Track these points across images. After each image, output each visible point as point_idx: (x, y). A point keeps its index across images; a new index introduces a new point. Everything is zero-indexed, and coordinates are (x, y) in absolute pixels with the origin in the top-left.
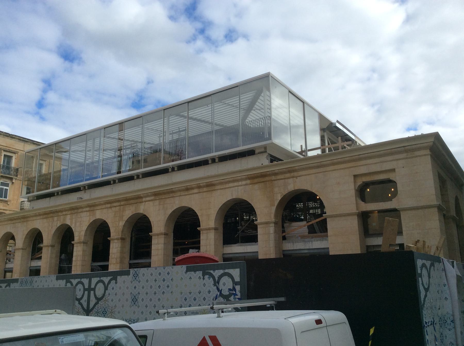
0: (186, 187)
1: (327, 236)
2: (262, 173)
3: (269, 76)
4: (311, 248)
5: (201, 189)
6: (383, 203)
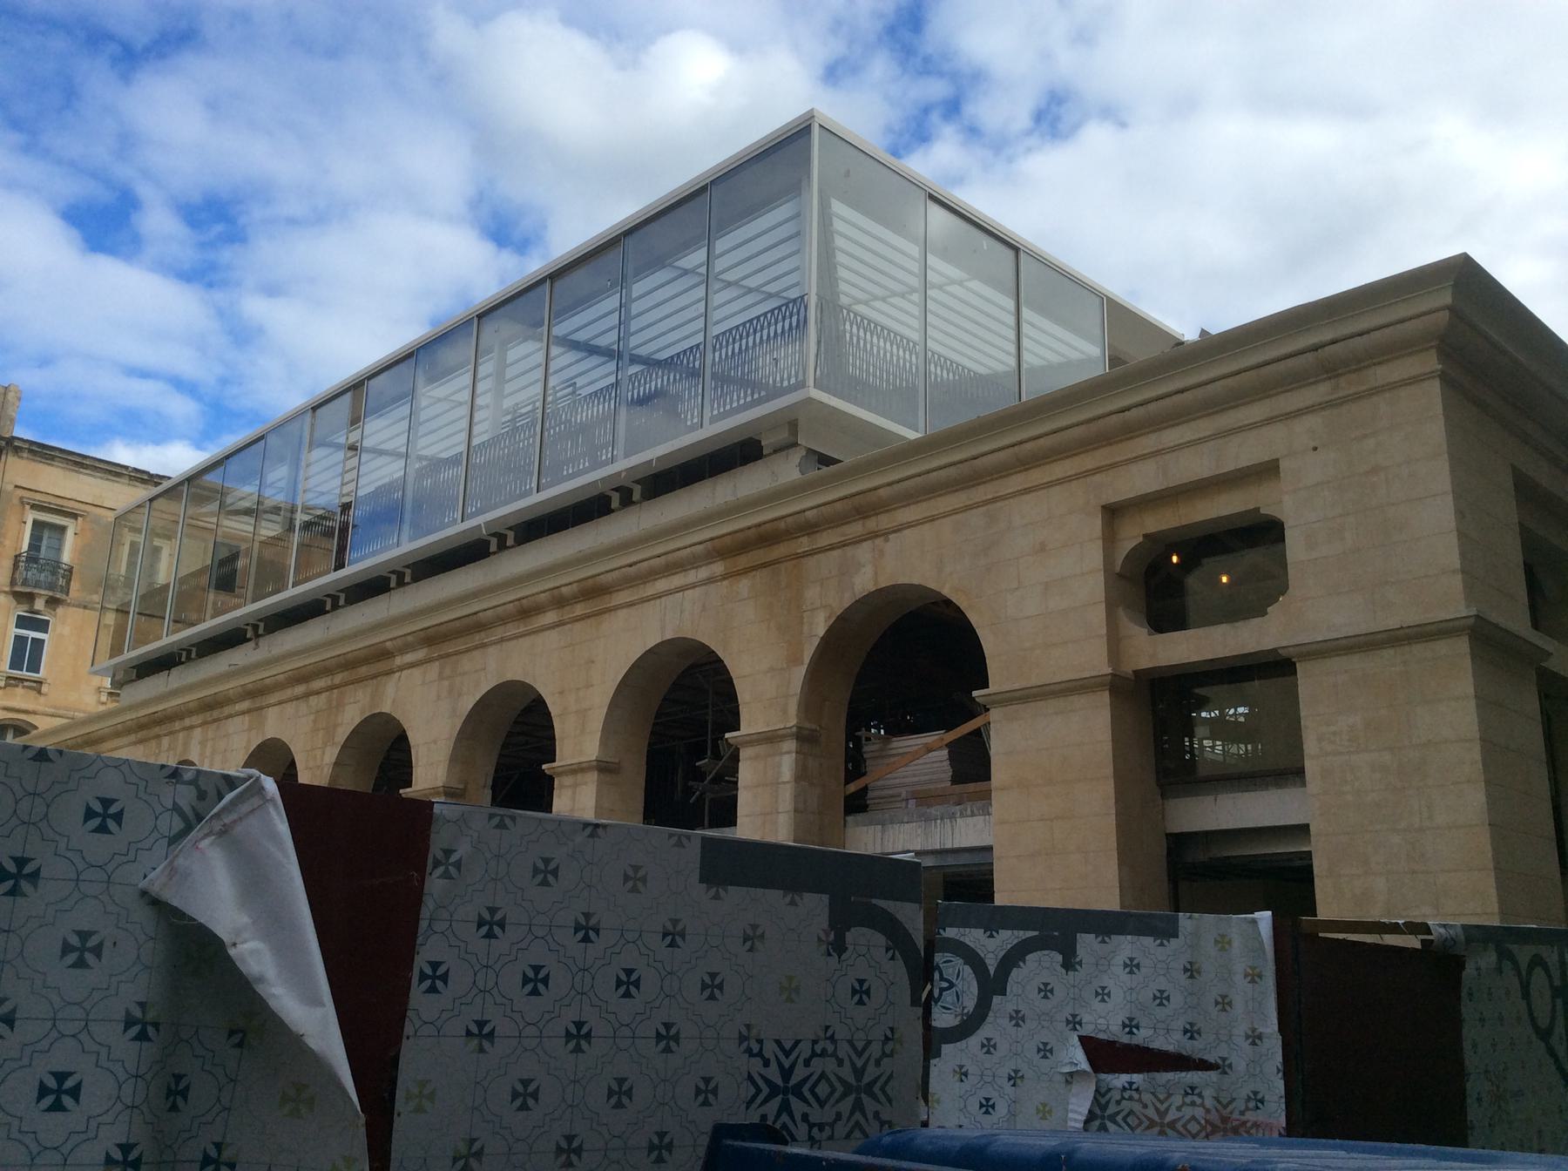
0: (516, 603)
1: (986, 796)
3: (810, 125)
4: (949, 846)
5: (568, 608)
6: (1224, 626)
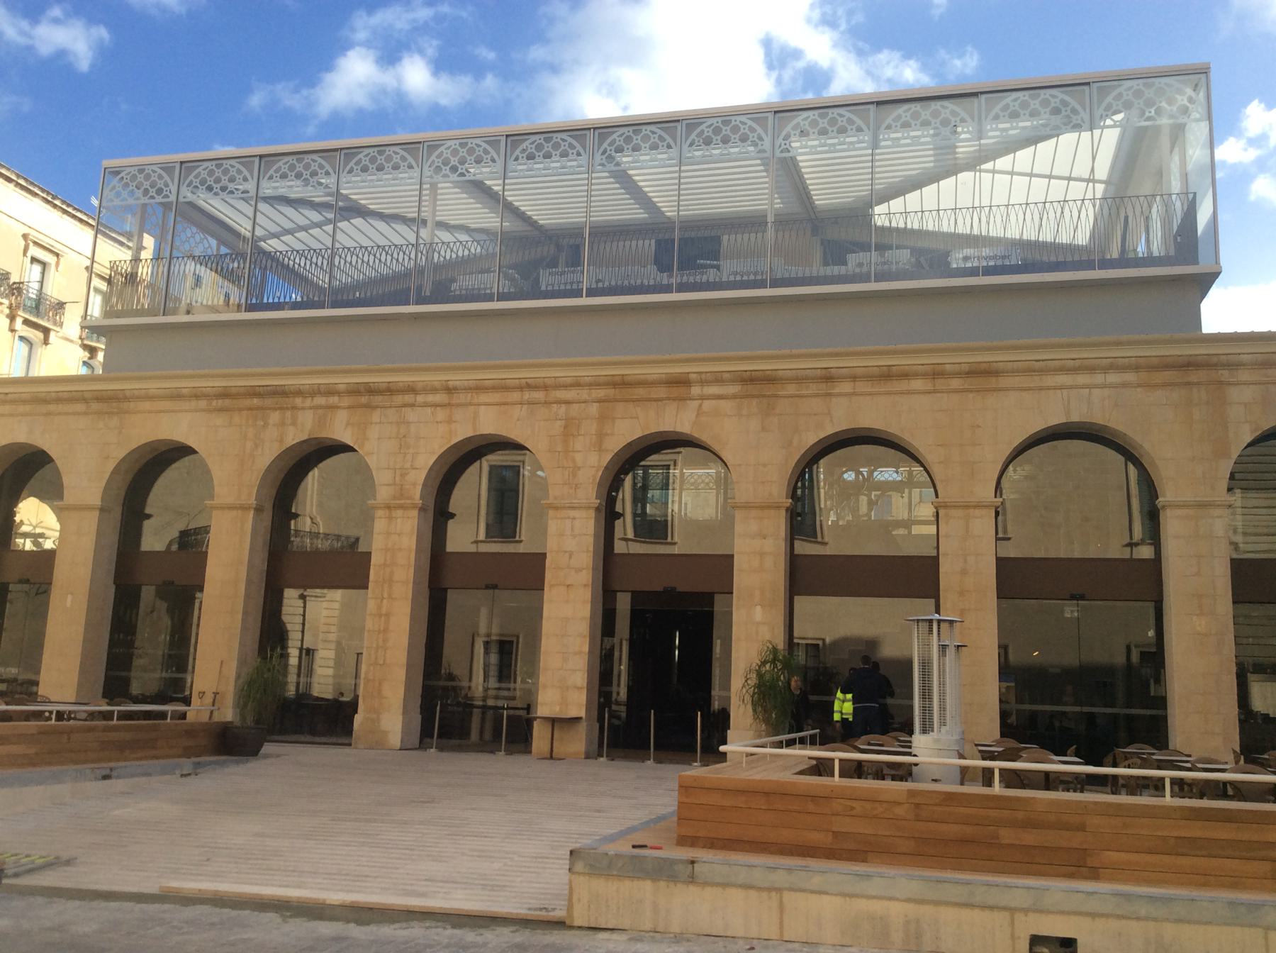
2: (1191, 355)
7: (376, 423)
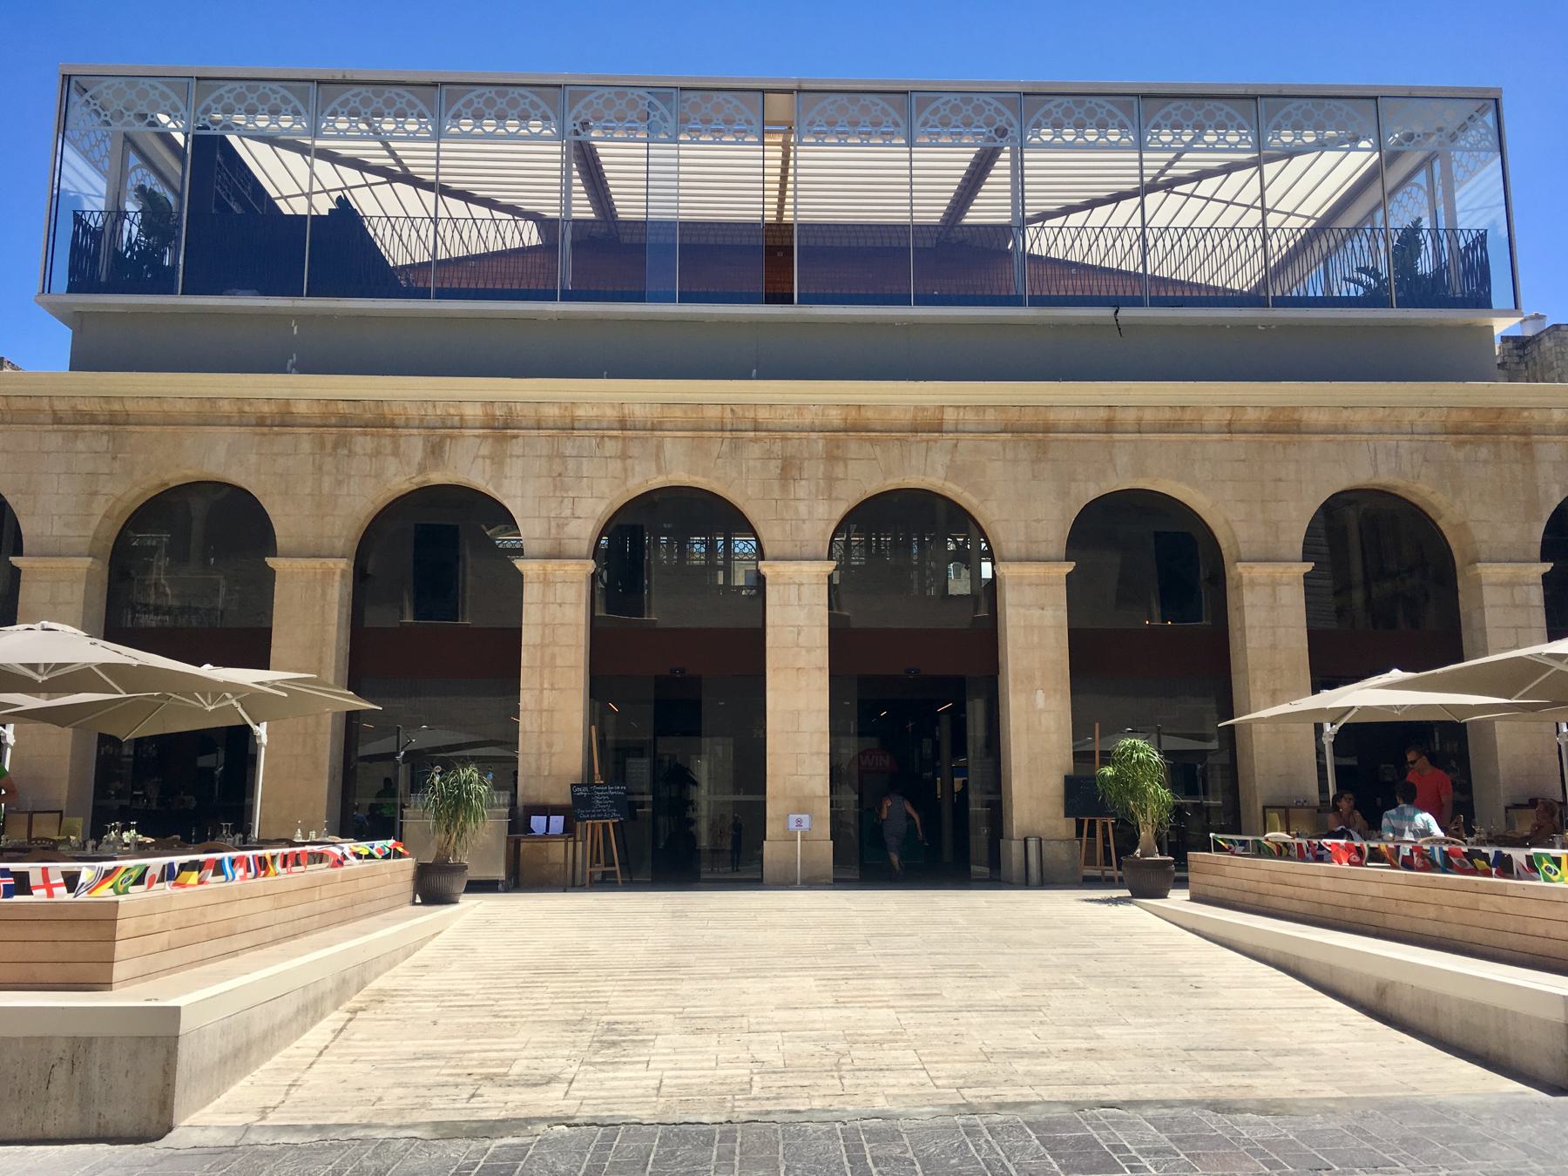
7: (518, 457)
